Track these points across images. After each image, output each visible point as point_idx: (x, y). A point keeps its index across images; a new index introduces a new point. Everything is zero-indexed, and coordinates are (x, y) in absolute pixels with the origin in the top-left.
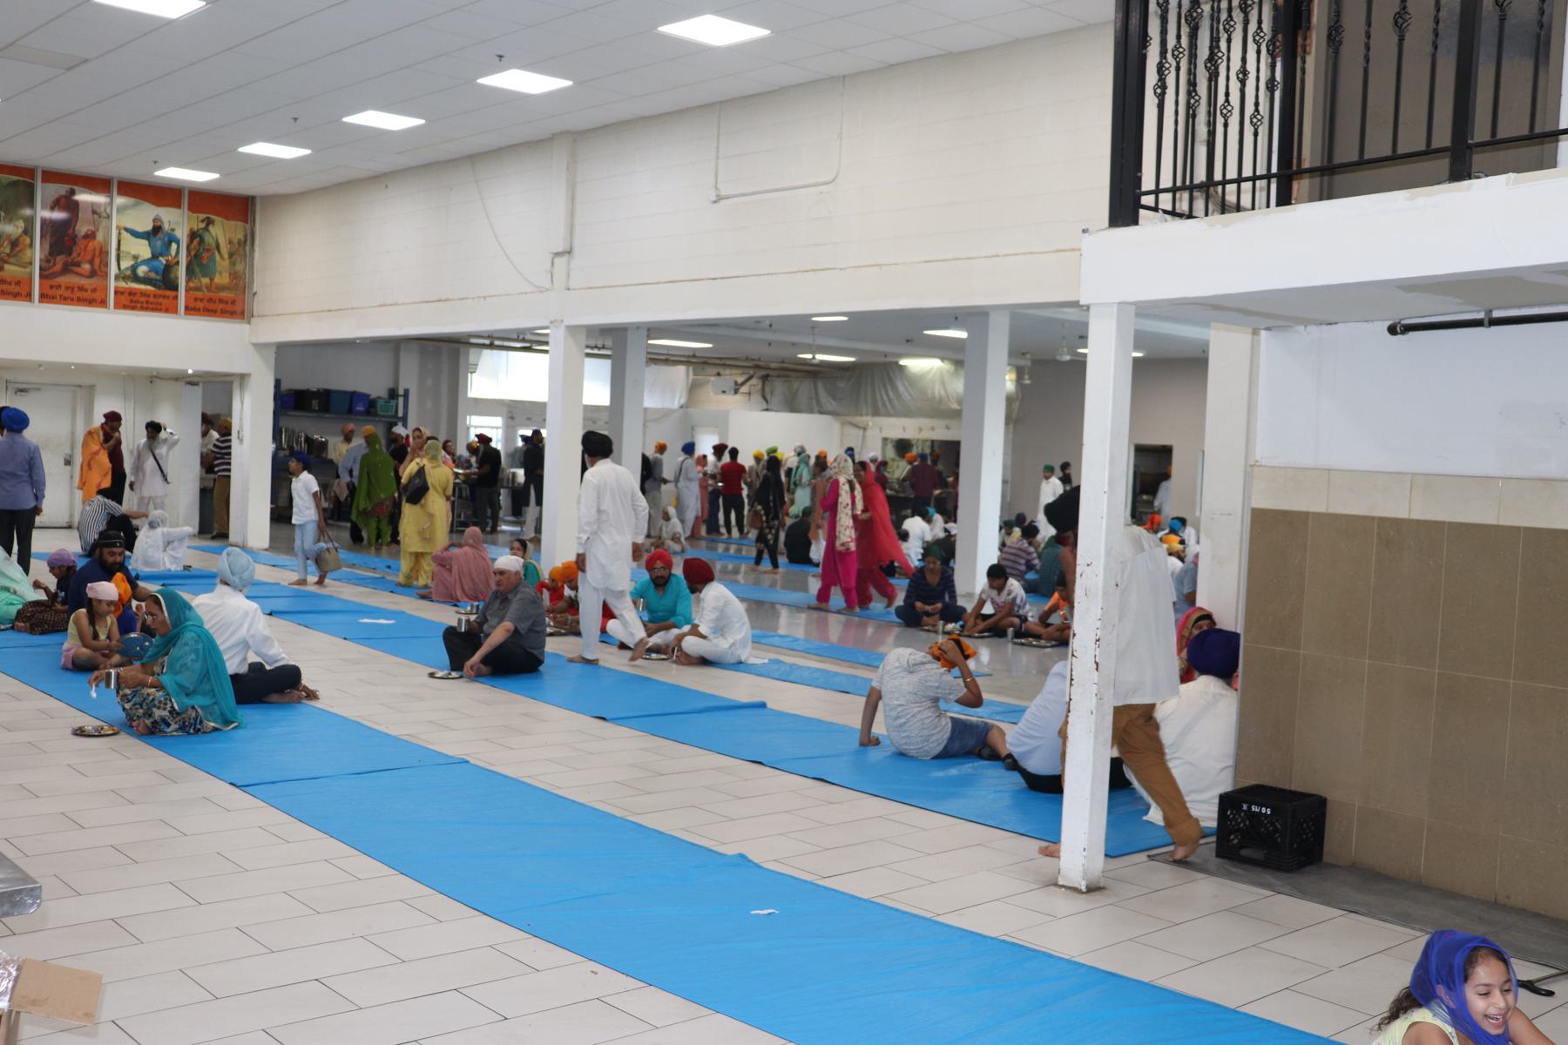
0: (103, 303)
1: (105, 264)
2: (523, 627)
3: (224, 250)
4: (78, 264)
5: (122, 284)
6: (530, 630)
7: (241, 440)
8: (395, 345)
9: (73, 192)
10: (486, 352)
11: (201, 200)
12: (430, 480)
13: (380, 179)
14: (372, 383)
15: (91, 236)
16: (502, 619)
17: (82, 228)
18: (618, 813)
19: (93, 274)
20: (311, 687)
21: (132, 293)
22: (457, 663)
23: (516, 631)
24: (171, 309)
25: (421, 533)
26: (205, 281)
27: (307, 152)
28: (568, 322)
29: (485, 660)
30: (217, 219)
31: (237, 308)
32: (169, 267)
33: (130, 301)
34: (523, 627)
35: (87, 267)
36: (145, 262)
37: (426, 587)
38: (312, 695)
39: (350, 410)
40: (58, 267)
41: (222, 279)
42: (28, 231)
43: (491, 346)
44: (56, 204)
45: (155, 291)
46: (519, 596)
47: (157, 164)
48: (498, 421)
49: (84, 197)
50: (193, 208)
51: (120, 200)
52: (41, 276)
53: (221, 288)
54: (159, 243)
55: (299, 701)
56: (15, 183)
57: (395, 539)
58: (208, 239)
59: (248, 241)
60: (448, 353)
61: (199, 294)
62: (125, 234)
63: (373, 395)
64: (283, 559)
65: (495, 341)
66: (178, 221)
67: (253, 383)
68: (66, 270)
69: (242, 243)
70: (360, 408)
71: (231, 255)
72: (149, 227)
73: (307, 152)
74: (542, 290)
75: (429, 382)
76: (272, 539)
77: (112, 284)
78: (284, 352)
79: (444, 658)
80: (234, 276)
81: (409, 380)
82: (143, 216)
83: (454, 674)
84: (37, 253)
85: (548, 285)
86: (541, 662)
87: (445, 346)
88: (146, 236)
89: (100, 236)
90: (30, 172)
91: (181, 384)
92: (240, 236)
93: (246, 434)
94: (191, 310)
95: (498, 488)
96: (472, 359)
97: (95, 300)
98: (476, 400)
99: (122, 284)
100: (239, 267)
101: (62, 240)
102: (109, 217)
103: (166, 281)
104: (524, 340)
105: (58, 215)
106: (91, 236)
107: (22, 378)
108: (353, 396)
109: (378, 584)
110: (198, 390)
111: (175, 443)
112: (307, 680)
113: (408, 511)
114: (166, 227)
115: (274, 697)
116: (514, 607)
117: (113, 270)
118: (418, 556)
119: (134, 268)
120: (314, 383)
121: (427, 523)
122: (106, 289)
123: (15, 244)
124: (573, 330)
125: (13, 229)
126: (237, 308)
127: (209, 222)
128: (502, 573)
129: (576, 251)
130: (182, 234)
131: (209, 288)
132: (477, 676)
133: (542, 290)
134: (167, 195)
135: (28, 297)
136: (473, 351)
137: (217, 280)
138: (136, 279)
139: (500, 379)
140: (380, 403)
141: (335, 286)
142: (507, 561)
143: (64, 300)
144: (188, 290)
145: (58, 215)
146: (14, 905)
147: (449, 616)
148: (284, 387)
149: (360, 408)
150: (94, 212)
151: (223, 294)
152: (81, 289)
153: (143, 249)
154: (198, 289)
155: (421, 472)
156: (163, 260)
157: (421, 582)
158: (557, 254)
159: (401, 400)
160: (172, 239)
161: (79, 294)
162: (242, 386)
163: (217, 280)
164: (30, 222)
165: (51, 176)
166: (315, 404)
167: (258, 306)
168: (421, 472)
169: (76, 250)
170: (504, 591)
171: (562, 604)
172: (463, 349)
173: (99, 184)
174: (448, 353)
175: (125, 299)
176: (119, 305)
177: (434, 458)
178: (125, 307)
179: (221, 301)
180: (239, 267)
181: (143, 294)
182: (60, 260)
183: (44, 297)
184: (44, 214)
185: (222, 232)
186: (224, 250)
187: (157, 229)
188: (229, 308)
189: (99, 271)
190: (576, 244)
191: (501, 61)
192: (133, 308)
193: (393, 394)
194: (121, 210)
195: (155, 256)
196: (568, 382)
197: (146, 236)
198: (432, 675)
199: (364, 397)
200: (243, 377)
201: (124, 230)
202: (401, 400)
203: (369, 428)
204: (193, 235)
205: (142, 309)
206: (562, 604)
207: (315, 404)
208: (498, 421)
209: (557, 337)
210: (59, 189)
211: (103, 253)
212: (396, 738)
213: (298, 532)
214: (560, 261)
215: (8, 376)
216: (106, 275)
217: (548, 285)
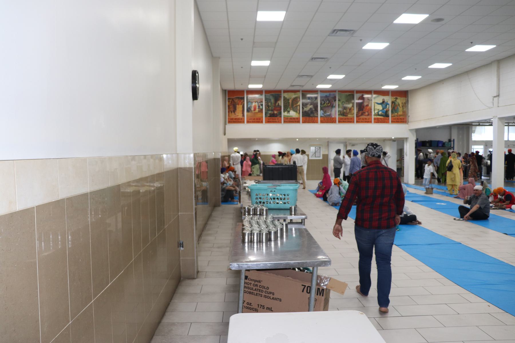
0: (371, 122)
1: (371, 112)
2: (482, 206)
3: (401, 105)
4: (365, 113)
5: (376, 117)
6: (485, 207)
7: (406, 155)
8: (450, 127)
9: (363, 95)
10: (478, 127)
11: (394, 93)
12: (453, 164)
13: (441, 81)
14: (444, 138)
15: (367, 105)
16: (476, 204)
17: (365, 104)
18: (506, 262)
19: (368, 115)
20: (420, 221)
21: (378, 119)
22: (462, 216)
23: (480, 208)
24: (387, 122)
25: (451, 179)
26: (396, 114)
27: (420, 77)
28: (499, 116)
29: (471, 215)
30: (398, 97)
31: (405, 120)
32: (387, 111)
33: (377, 121)
34: (482, 206)
35: (367, 113)
36: (381, 111)
37: (457, 194)
38: (420, 223)
39: (438, 146)
40: (360, 114)
41: (400, 113)
42: (353, 106)
43: (479, 125)
44: (359, 98)
45: (383, 118)
46: (481, 197)
47: (382, 85)
48: (482, 147)
49: (366, 96)
50: (392, 95)
51: (374, 96)
52: (357, 117)
53: (400, 115)
54: (384, 106)
55: (416, 224)
56: (350, 95)
57: (445, 181)
58: (397, 103)
59: (407, 102)
60: (466, 128)
61: (395, 118)
62: (376, 104)
63: (444, 141)
64: (418, 187)
65: (480, 124)
66: (389, 99)
67: (409, 140)
68: (362, 114)
69: (405, 103)
70: (440, 145)
71: (403, 106)
72: (381, 101)
73: (420, 77)
74: (490, 108)
75: (461, 137)
76: (415, 182)
77: (373, 117)
78: (417, 131)
79: (458, 214)
80: (404, 112)
81: (454, 136)
82: (380, 99)
83: (461, 219)
84: (355, 111)
85: (492, 106)
86: (488, 217)
87: (465, 126)
88: (381, 104)
89: (370, 105)
90: (280, 91)
91: (391, 141)
92: (404, 101)
93: (408, 154)
94: (393, 122)
95: (476, 165)
96: (473, 129)
97: (369, 121)
98: (475, 141)
99: (376, 117)
100: (405, 110)
101: (361, 107)
102: (372, 100)
103: (386, 115)
104: (489, 123)
105: (360, 101)
106: (367, 105)
107: (354, 142)
108: (438, 142)
109: (443, 194)
110: (396, 143)
111: (390, 157)
112: (419, 219)
113: (448, 173)
114: (386, 101)
115: (410, 223)
116: (479, 201)
117: (373, 113)
118: (453, 186)
119: (378, 113)
120: (427, 139)
121: (456, 176)
122: (371, 118)
123: (350, 109)
124: (501, 119)
125: (350, 106)
126: (405, 120)
127: (396, 99)
128: (477, 190)
129: (501, 95)
130: (390, 102)
131: (397, 116)
132: (468, 220)
133: (490, 108)
134: (385, 93)
135: (353, 122)
136: (473, 127)
137: (399, 113)
138: (379, 115)
139: (481, 135)
140: (446, 143)
141: (432, 112)
142: (478, 187)
143: (362, 122)
144: (392, 117)
145: (360, 101)
146: (325, 264)
147: (460, 202)
148: (419, 140)
149: (440, 145)
150: (368, 99)
151: (401, 117)
152: (366, 119)
153: (380, 107)
154: (394, 116)
155: (451, 161)
156: (385, 110)
157: (455, 193)
158: (495, 97)
159: (452, 142)
160: (387, 104)
161: (365, 120)
162: (406, 141)
163: (399, 113)
164: (353, 104)
165: (358, 92)
166: (428, 145)
167: (410, 119)
168: (451, 161)
169: (364, 109)
170: (477, 195)
171: (497, 200)
172: (470, 127)
173: (369, 92)
174: (466, 128)
175: (376, 121)
176: (375, 122)
177: (454, 157)
178: (376, 122)
179: (401, 119)
180: (405, 110)
181: (381, 119)
182: (361, 112)
183: (357, 122)
184: (357, 101)
185: (400, 101)
186: (401, 105)
187: (383, 102)
188: (403, 120)
189: (370, 114)
190: (501, 93)
191: (472, 44)
192: (378, 122)
193: (450, 141)
194: (375, 98)
195: (383, 109)
196: (499, 134)
197: (381, 104)
198: (455, 219)
199: (441, 142)
200: (407, 139)
201: (375, 103)
202: (452, 142)
203: (442, 151)
204: (393, 102)
205: (381, 122)
206: (497, 200)
207: (428, 145)
208: (482, 147)
209: (495, 121)
210: (359, 95)
211: (371, 109)
212: (441, 236)
213: (424, 180)
214: (496, 99)
215: (351, 142)
216: (371, 115)
217: (492, 106)
